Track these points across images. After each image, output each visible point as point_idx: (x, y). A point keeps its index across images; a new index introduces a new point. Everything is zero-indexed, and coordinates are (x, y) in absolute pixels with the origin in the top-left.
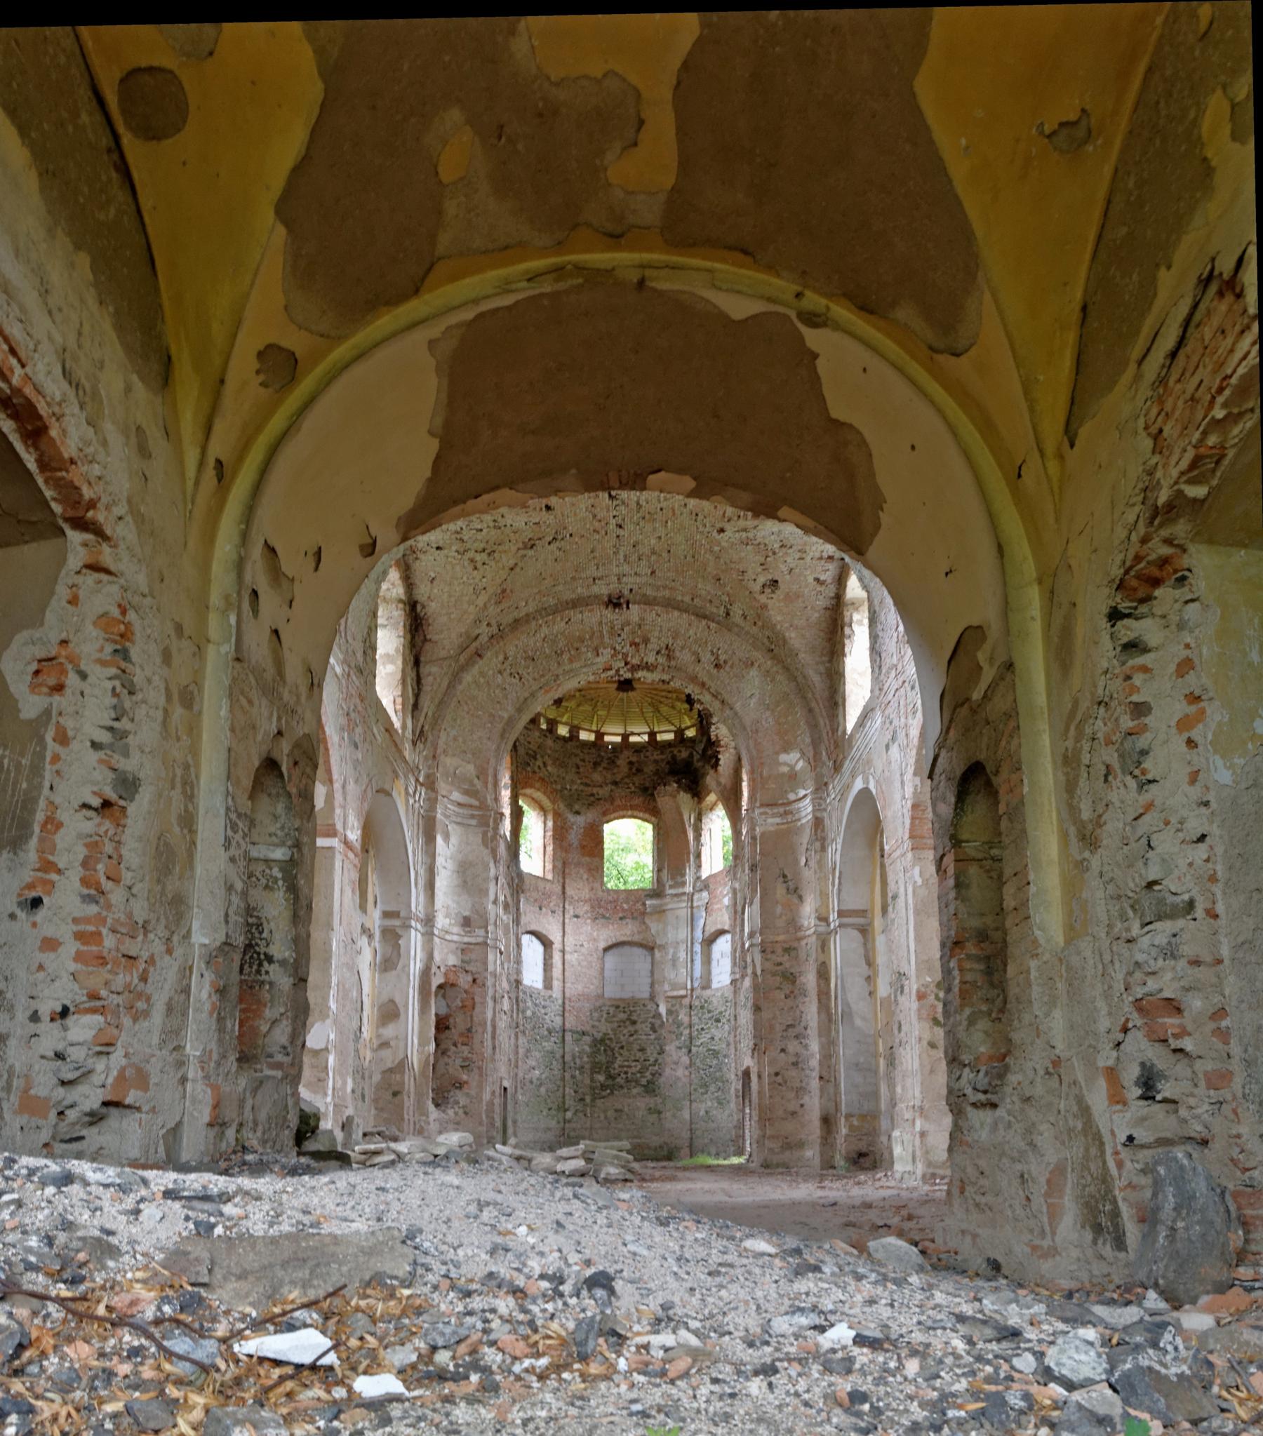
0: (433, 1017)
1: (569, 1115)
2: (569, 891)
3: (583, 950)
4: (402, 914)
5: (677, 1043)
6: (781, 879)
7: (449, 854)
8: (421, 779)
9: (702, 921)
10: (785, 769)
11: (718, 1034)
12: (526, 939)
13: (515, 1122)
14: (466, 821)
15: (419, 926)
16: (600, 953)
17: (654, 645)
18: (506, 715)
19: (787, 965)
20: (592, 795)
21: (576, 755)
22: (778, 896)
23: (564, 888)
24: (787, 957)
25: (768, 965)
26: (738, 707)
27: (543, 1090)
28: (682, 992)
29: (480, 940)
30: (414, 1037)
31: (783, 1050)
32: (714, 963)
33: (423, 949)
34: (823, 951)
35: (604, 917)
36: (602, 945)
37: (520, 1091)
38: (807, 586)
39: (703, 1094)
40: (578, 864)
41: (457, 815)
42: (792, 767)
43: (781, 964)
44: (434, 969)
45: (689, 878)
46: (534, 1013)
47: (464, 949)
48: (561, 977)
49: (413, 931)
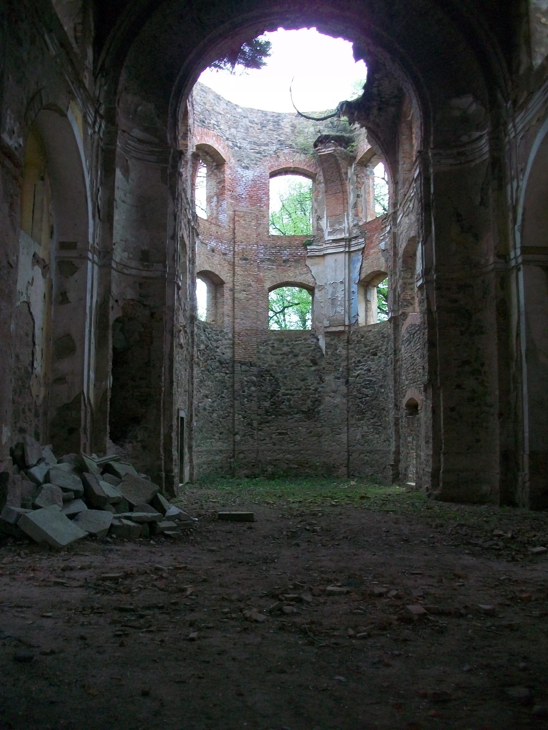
0: (111, 351)
1: (238, 438)
4: (79, 245)
8: (102, 112)
10: (457, 113)
11: (373, 366)
13: (190, 448)
15: (96, 258)
27: (215, 415)
28: (341, 328)
30: (90, 375)
31: (459, 386)
33: (100, 284)
34: (503, 288)
37: (195, 418)
39: (359, 420)
43: (456, 301)
44: (111, 303)
46: (207, 346)
47: (141, 284)
48: (231, 314)
49: (90, 264)
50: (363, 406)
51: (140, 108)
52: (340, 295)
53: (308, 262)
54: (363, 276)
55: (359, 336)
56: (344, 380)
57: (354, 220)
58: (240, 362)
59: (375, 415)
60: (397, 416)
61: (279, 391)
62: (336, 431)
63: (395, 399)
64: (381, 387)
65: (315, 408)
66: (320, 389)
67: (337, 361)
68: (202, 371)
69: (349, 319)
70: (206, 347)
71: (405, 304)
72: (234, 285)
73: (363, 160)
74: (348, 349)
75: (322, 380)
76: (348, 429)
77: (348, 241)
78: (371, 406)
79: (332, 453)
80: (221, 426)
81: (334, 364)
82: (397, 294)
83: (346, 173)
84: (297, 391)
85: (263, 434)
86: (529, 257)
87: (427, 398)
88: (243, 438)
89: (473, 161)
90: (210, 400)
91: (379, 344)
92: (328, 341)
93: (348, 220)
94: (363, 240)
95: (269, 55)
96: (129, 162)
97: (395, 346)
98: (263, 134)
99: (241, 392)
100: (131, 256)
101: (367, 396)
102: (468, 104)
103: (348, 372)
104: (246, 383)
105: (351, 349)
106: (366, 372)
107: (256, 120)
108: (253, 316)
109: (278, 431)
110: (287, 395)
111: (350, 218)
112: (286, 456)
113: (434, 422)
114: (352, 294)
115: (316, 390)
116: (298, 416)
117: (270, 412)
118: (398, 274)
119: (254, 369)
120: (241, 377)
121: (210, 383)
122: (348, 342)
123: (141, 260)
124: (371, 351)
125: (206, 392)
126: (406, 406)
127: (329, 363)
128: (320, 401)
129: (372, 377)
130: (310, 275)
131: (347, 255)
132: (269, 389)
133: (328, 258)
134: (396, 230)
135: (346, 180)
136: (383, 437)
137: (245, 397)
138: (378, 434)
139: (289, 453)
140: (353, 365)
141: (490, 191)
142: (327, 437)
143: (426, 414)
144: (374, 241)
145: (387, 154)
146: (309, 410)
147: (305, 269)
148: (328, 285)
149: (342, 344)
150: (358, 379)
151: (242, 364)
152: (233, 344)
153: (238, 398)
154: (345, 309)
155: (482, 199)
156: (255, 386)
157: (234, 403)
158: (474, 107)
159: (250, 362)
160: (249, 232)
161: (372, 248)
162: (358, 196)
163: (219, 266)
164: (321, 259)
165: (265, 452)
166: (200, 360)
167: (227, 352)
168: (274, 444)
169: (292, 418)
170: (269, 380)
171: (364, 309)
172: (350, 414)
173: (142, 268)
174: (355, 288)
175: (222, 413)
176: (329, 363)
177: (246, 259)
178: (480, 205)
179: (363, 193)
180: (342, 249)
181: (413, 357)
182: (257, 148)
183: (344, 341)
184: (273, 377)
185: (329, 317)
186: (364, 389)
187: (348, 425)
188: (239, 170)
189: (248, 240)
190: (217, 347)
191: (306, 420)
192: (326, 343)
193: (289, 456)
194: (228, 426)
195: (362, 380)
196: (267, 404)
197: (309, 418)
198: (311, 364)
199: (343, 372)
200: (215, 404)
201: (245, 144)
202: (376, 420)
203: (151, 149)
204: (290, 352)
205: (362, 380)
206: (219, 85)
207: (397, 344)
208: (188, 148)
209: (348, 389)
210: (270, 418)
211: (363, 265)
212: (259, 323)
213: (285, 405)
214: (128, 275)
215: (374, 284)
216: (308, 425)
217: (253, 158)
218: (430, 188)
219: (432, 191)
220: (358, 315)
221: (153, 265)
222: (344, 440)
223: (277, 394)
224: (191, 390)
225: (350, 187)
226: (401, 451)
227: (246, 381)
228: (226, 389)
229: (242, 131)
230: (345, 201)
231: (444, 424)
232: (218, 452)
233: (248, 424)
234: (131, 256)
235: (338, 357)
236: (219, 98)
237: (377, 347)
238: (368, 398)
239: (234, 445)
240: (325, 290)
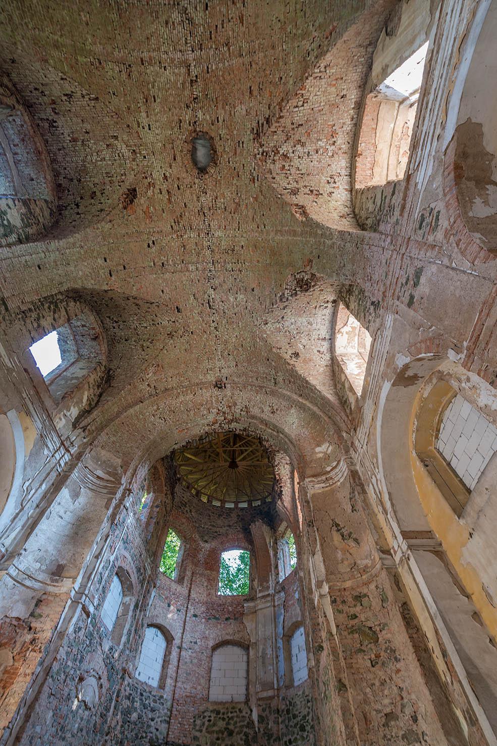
2: (193, 595)
3: (196, 647)
6: (335, 528)
7: (72, 507)
9: (282, 617)
10: (321, 455)
12: (150, 633)
16: (209, 652)
17: (239, 407)
18: (152, 437)
20: (216, 532)
21: (209, 510)
22: (336, 543)
23: (190, 591)
25: (342, 618)
26: (286, 430)
32: (294, 659)
34: (399, 589)
35: (215, 618)
36: (211, 643)
38: (314, 355)
40: (201, 575)
41: (94, 484)
45: (271, 583)
46: (140, 717)
48: (174, 674)
86: (413, 541)
111: (273, 577)
158: (330, 448)
192: (258, 715)
212: (199, 687)
214: (28, 587)
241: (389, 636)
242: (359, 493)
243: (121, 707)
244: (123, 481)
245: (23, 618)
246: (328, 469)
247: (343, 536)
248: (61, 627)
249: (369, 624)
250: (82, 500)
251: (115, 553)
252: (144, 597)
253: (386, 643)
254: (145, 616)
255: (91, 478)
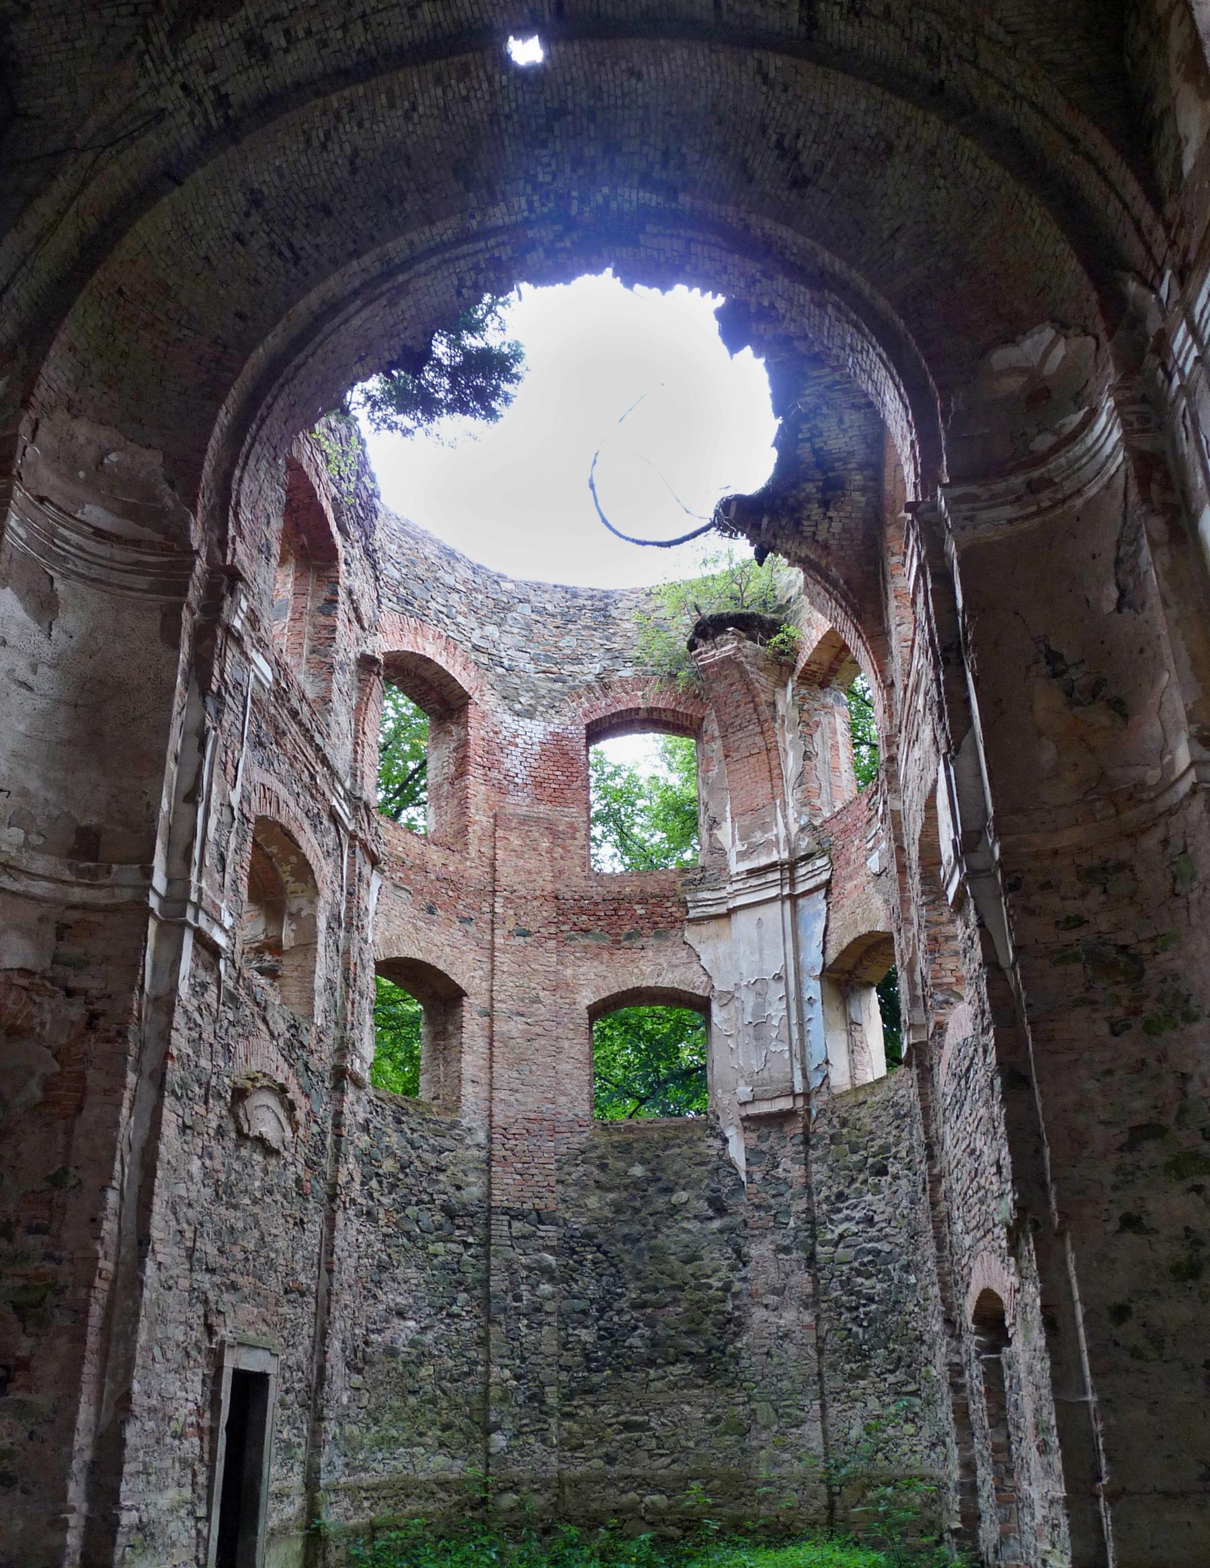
1: (499, 1441)
5: (778, 1238)
6: (1045, 669)
7: (47, 651)
10: (1014, 384)
11: (879, 1205)
14: (115, 577)
19: (1103, 923)
24: (1095, 898)
28: (785, 1104)
29: (126, 895)
31: (1131, 1223)
36: (587, 998)
39: (854, 1377)
42: (1032, 373)
48: (483, 1077)
50: (860, 1330)
51: (113, 457)
52: (776, 1011)
53: (691, 934)
54: (832, 954)
55: (835, 1121)
56: (803, 1255)
57: (800, 814)
58: (506, 1211)
59: (900, 1359)
60: (956, 1359)
61: (621, 1295)
62: (789, 1415)
63: (944, 1300)
64: (906, 1268)
65: (726, 1345)
66: (737, 1286)
67: (780, 1199)
68: (385, 1235)
69: (805, 1077)
70: (403, 1168)
71: (940, 997)
72: (492, 998)
73: (814, 667)
74: (807, 1164)
75: (742, 1259)
76: (823, 1407)
77: (790, 867)
78: (884, 1330)
79: (782, 1488)
80: (445, 1404)
81: (771, 1207)
82: (918, 979)
83: (773, 705)
84: (673, 1293)
85: (576, 1427)
87: (1020, 1272)
88: (514, 1443)
89: (1079, 492)
90: (411, 1324)
91: (891, 1139)
92: (753, 1142)
93: (785, 817)
94: (825, 860)
95: (517, 377)
96: (56, 585)
97: (926, 1133)
98: (568, 638)
99: (509, 1298)
100: (36, 840)
101: (871, 1299)
102: (1044, 349)
103: (812, 1230)
104: (524, 1273)
105: (816, 1160)
106: (861, 1227)
107: (549, 607)
108: (546, 1081)
109: (622, 1418)
110: (644, 1305)
112: (647, 1499)
113: (1055, 1365)
114: (806, 1007)
115: (726, 1288)
116: (677, 1369)
117: (596, 1360)
118: (916, 921)
119: (549, 1232)
120: (512, 1254)
121: (412, 1272)
122: (806, 1142)
123: (72, 854)
124: (870, 1160)
125: (399, 1299)
126: (974, 1322)
127: (758, 1207)
128: (740, 1324)
129: (879, 1240)
130: (696, 967)
131: (788, 905)
132: (593, 1290)
133: (741, 918)
134: (898, 805)
135: (774, 719)
136: (926, 1432)
137: (520, 1314)
138: (913, 1421)
139: (657, 1490)
140: (825, 1207)
141: (1146, 553)
142: (764, 1436)
143: (1027, 1340)
144: (853, 857)
145: (858, 617)
146: (709, 1353)
147: (684, 954)
148: (744, 990)
149: (790, 1149)
150: (840, 1250)
151: (513, 1217)
152: (489, 1161)
153: (502, 1317)
154: (790, 1050)
155: (1122, 592)
156: (552, 1280)
157: (488, 1333)
158: (1060, 351)
159: (537, 1211)
160: (532, 865)
161: (850, 878)
162: (807, 756)
163: (448, 949)
164: (723, 922)
165: (582, 1486)
166: (380, 1204)
167: (469, 1184)
168: (610, 1460)
169: (663, 1378)
170: (594, 1263)
171: (844, 1048)
172: (829, 1358)
173: (73, 878)
174: (813, 989)
175: (451, 1363)
176: (758, 1207)
177: (525, 934)
178: (1119, 609)
179: (818, 749)
180: (773, 892)
181: (973, 1151)
182: (555, 669)
183: (796, 1141)
184: (605, 1253)
185: (751, 1074)
186: (860, 1280)
187: (822, 1393)
188: (508, 718)
189: (531, 886)
190: (440, 1170)
191: (700, 1381)
193: (655, 1498)
194: (468, 1403)
195: (851, 1252)
196: (586, 1335)
197: (709, 1375)
198: (710, 1213)
199: (797, 1230)
200: (429, 1337)
201: (522, 661)
202: (900, 1375)
203: (137, 556)
204: (649, 1181)
205: (851, 1252)
206: (406, 467)
207: (934, 1126)
208: (337, 635)
209: (816, 1281)
210: (596, 1379)
211: (831, 925)
212: (562, 1100)
213: (642, 1337)
214: (15, 894)
215: (867, 978)
216: (709, 1396)
217: (543, 692)
218: (955, 598)
219: (960, 603)
220: (827, 1062)
221: (109, 872)
222: (814, 1445)
223: (616, 1305)
224: (323, 1291)
225: (788, 739)
226: (979, 1483)
227: (530, 1269)
228: (465, 1290)
229: (516, 631)
230: (774, 775)
231: (1094, 1374)
232: (435, 1488)
233: (532, 1398)
234: (36, 840)
235: (783, 1188)
236: (451, 556)
237: (885, 1148)
238: (874, 1307)
239: (488, 1465)
240: (737, 1004)
241: (1179, 964)
242: (1154, 545)
243: (351, 1148)
244: (196, 537)
245: (39, 970)
246: (1043, 442)
247: (1069, 694)
248: (152, 986)
249: (1125, 938)
250: (70, 621)
251: (239, 783)
252: (350, 894)
253: (1164, 981)
254: (366, 942)
255: (74, 537)
